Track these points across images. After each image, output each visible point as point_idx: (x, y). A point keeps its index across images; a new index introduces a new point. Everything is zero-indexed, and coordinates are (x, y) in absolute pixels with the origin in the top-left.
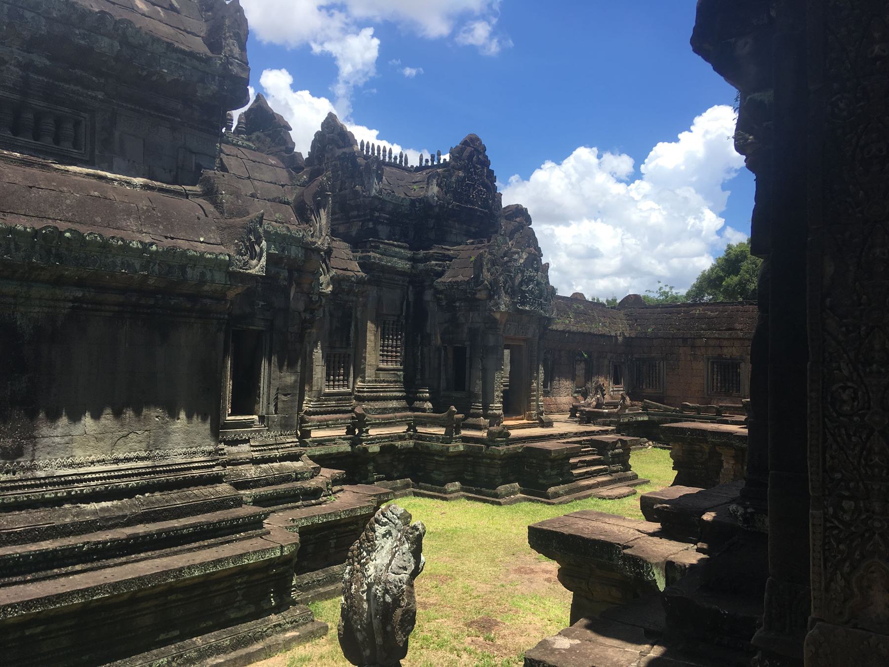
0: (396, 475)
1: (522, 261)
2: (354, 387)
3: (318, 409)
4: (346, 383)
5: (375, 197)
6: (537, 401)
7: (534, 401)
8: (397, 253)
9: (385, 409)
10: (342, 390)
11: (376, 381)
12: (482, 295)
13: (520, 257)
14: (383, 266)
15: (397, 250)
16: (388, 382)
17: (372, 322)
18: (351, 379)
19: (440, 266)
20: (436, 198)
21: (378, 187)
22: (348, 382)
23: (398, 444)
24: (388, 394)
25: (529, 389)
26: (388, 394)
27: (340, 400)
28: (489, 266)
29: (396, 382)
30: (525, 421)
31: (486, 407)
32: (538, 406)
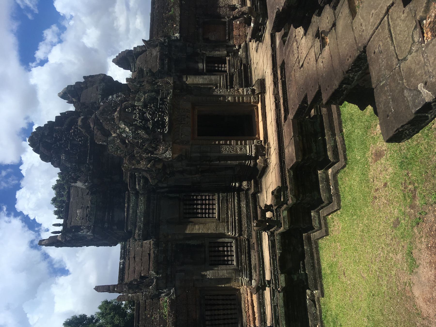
0: (301, 249)
1: (127, 129)
2: (232, 238)
3: (248, 273)
4: (229, 245)
5: (93, 232)
6: (243, 96)
7: (243, 99)
8: (133, 212)
9: (247, 217)
10: (234, 249)
11: (228, 222)
12: (160, 166)
13: (124, 131)
14: (144, 225)
15: (131, 211)
16: (227, 210)
17: (186, 229)
18: (227, 240)
19: (139, 181)
20: (86, 184)
21: (85, 230)
22: (228, 243)
23: (278, 255)
24: (236, 211)
25: (234, 104)
26: (236, 211)
27: (241, 250)
28: (134, 162)
29: (227, 200)
30: (259, 105)
31: (250, 158)
32: (247, 95)
